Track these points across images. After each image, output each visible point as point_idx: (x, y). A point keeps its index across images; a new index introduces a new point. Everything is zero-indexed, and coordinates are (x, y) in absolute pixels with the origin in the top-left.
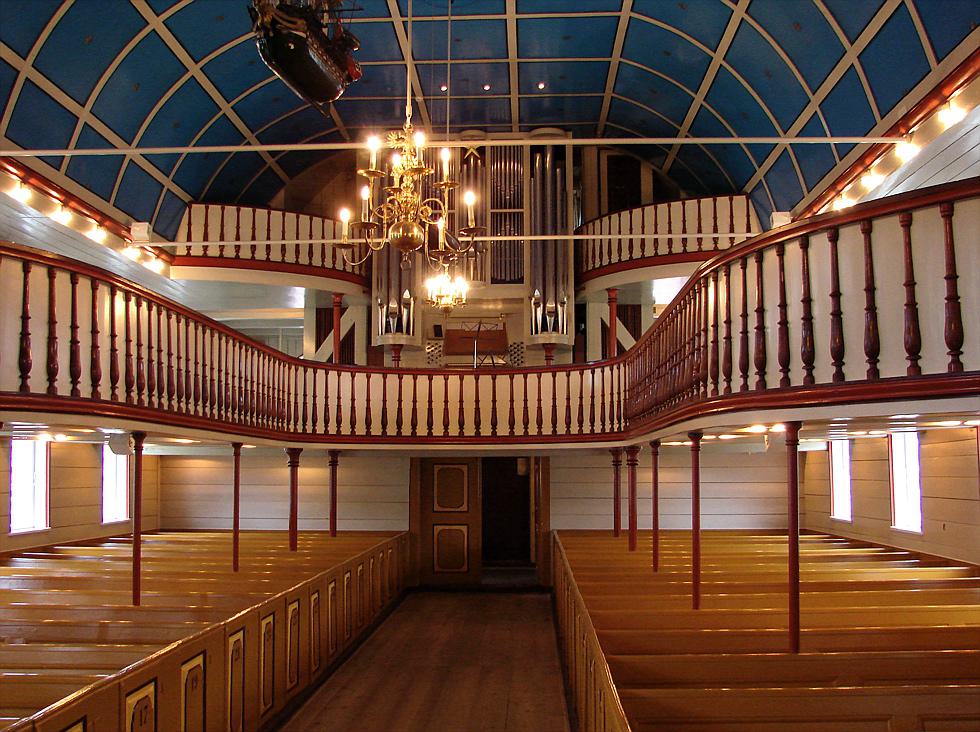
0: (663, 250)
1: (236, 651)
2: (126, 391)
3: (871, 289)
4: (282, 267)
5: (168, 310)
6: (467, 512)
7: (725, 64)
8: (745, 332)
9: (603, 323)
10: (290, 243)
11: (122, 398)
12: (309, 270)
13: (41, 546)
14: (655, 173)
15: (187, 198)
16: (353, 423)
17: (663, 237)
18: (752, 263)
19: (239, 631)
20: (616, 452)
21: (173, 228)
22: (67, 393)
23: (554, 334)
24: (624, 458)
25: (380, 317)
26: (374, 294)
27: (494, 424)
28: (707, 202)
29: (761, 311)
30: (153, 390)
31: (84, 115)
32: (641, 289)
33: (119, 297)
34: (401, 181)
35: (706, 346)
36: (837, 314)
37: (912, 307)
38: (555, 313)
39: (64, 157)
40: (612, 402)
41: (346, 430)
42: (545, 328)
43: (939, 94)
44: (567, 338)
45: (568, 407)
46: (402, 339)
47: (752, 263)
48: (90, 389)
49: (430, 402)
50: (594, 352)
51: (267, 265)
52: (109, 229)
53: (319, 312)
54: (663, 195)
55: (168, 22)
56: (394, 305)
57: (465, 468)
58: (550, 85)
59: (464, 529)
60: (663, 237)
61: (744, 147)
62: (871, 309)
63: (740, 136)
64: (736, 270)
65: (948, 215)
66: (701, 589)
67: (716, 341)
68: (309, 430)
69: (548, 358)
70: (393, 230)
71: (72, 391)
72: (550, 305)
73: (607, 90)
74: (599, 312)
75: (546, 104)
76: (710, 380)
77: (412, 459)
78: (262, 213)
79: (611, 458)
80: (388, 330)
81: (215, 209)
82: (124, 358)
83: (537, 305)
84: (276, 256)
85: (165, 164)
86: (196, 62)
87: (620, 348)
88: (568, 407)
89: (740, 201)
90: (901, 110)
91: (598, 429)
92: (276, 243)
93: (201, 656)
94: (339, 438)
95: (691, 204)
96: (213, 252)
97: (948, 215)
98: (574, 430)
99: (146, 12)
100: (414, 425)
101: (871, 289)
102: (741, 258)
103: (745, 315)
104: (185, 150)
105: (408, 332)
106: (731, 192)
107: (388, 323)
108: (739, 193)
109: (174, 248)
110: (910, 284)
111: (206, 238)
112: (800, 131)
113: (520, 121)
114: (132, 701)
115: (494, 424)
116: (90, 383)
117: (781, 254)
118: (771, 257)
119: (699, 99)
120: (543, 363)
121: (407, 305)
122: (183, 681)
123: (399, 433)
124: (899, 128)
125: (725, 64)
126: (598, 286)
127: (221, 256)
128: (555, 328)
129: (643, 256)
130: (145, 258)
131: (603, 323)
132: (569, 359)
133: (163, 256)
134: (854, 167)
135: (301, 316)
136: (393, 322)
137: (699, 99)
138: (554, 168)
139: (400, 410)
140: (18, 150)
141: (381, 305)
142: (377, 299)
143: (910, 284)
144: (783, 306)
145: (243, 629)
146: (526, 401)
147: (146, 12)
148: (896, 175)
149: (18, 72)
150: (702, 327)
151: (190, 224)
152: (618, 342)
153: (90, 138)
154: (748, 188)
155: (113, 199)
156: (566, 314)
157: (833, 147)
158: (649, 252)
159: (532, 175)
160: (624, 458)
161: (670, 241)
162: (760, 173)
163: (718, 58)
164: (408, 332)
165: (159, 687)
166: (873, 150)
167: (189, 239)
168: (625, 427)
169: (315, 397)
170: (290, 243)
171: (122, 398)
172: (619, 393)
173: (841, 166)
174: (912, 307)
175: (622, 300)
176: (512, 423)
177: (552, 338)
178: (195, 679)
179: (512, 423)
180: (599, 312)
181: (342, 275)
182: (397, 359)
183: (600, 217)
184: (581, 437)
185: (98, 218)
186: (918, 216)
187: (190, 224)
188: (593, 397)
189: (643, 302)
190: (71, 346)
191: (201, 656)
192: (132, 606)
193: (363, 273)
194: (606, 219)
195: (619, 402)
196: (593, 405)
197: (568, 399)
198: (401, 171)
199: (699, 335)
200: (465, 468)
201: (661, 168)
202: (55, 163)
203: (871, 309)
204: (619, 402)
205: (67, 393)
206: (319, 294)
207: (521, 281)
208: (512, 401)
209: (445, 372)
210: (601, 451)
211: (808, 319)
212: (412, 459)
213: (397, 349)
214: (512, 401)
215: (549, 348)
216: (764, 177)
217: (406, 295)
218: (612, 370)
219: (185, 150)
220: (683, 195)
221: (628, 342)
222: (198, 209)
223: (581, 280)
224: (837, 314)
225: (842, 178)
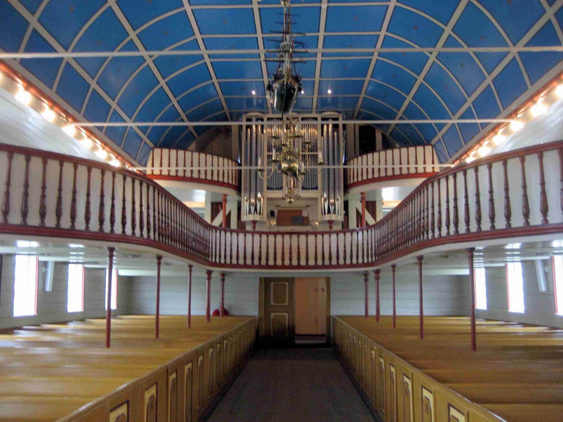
0: (390, 173)
3: (507, 189)
4: (191, 180)
5: (171, 199)
6: (288, 306)
8: (448, 209)
9: (357, 211)
10: (203, 169)
11: (152, 238)
12: (212, 182)
13: (81, 318)
14: (383, 135)
15: (152, 145)
16: (238, 259)
17: (383, 167)
18: (451, 178)
20: (366, 274)
21: (145, 160)
23: (329, 215)
24: (372, 276)
25: (245, 206)
26: (243, 194)
27: (307, 260)
28: (412, 149)
29: (456, 199)
32: (377, 193)
35: (428, 216)
36: (492, 200)
37: (525, 197)
38: (334, 204)
40: (368, 248)
41: (234, 261)
42: (329, 212)
43: (532, 99)
44: (340, 218)
45: (345, 251)
46: (257, 218)
47: (451, 178)
49: (275, 248)
50: (353, 224)
51: (184, 179)
52: (120, 160)
53: (213, 204)
54: (387, 145)
56: (253, 200)
57: (287, 284)
58: (334, 92)
59: (286, 315)
60: (383, 167)
61: (434, 125)
62: (507, 198)
64: (443, 181)
65: (541, 158)
67: (433, 214)
68: (218, 261)
69: (331, 227)
72: (332, 201)
73: (316, 77)
74: (356, 205)
75: (329, 100)
76: (430, 231)
77: (260, 279)
78: (181, 153)
79: (362, 278)
80: (250, 212)
81: (166, 151)
83: (325, 200)
84: (195, 175)
85: (142, 129)
87: (367, 224)
88: (345, 251)
89: (429, 149)
90: (513, 107)
91: (360, 261)
92: (196, 169)
94: (225, 265)
95: (404, 150)
96: (173, 173)
97: (541, 158)
98: (354, 261)
100: (267, 259)
101: (507, 189)
102: (453, 174)
103: (448, 202)
105: (260, 214)
106: (424, 144)
107: (250, 209)
108: (429, 144)
109: (145, 171)
110: (525, 187)
111: (161, 165)
113: (317, 108)
115: (307, 260)
117: (465, 174)
118: (460, 176)
120: (328, 229)
121: (260, 200)
123: (260, 263)
124: (513, 114)
126: (355, 193)
127: (177, 175)
128: (334, 212)
129: (362, 180)
131: (357, 211)
132: (340, 228)
134: (489, 133)
135: (203, 206)
136: (252, 209)
138: (333, 132)
139: (260, 252)
141: (246, 200)
142: (244, 197)
143: (525, 187)
144: (466, 197)
146: (323, 247)
148: (511, 136)
151: (153, 158)
152: (366, 221)
154: (433, 142)
156: (339, 204)
157: (479, 125)
158: (383, 174)
159: (322, 135)
160: (372, 276)
161: (386, 169)
162: (440, 135)
163: (420, 79)
164: (260, 214)
166: (498, 125)
167: (153, 166)
168: (375, 260)
169: (220, 245)
170: (203, 169)
171: (152, 238)
172: (372, 244)
173: (482, 132)
174: (525, 197)
175: (369, 198)
176: (316, 259)
177: (333, 217)
179: (316, 259)
180: (356, 205)
181: (228, 185)
182: (254, 227)
183: (353, 158)
184: (352, 266)
185: (116, 155)
186: (528, 158)
187: (153, 158)
188: (358, 246)
189: (377, 200)
193: (237, 185)
194: (360, 158)
195: (372, 248)
196: (358, 250)
197: (345, 247)
200: (287, 284)
201: (386, 132)
203: (507, 198)
204: (372, 248)
206: (213, 194)
207: (317, 188)
208: (316, 248)
209: (275, 234)
210: (358, 273)
211: (478, 202)
212: (260, 279)
213: (254, 222)
214: (316, 248)
215: (331, 222)
216: (442, 137)
217: (259, 195)
218: (367, 232)
220: (397, 145)
221: (371, 221)
222: (157, 151)
223: (347, 188)
224: (492, 200)
225: (483, 138)
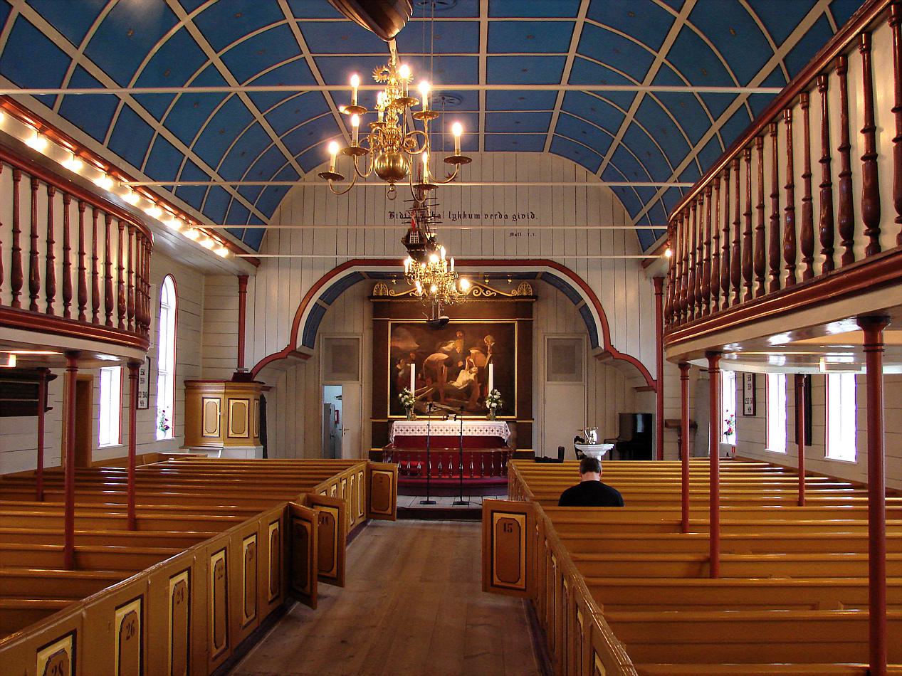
1: (250, 552)
2: (118, 318)
7: (634, 120)
19: (252, 535)
22: (61, 315)
30: (20, 286)
31: (77, 56)
33: (114, 225)
34: (385, 114)
35: (708, 259)
39: (57, 95)
48: (62, 309)
52: (229, 248)
55: (195, 20)
63: (630, 187)
66: (865, 596)
70: (380, 160)
71: (13, 302)
82: (62, 266)
86: (293, 156)
93: (139, 601)
99: (179, 10)
104: (267, 184)
112: (763, 82)
114: (121, 614)
116: (11, 290)
119: (630, 116)
122: (171, 594)
125: (634, 120)
130: (202, 238)
133: (228, 245)
137: (630, 116)
140: (16, 88)
145: (256, 533)
147: (179, 10)
149: (71, 59)
150: (705, 241)
153: (82, 78)
155: (202, 209)
165: (78, 640)
178: (131, 628)
190: (13, 253)
191: (139, 601)
192: (394, 436)
198: (387, 104)
199: (701, 249)
202: (169, 189)
205: (61, 315)
219: (267, 184)
